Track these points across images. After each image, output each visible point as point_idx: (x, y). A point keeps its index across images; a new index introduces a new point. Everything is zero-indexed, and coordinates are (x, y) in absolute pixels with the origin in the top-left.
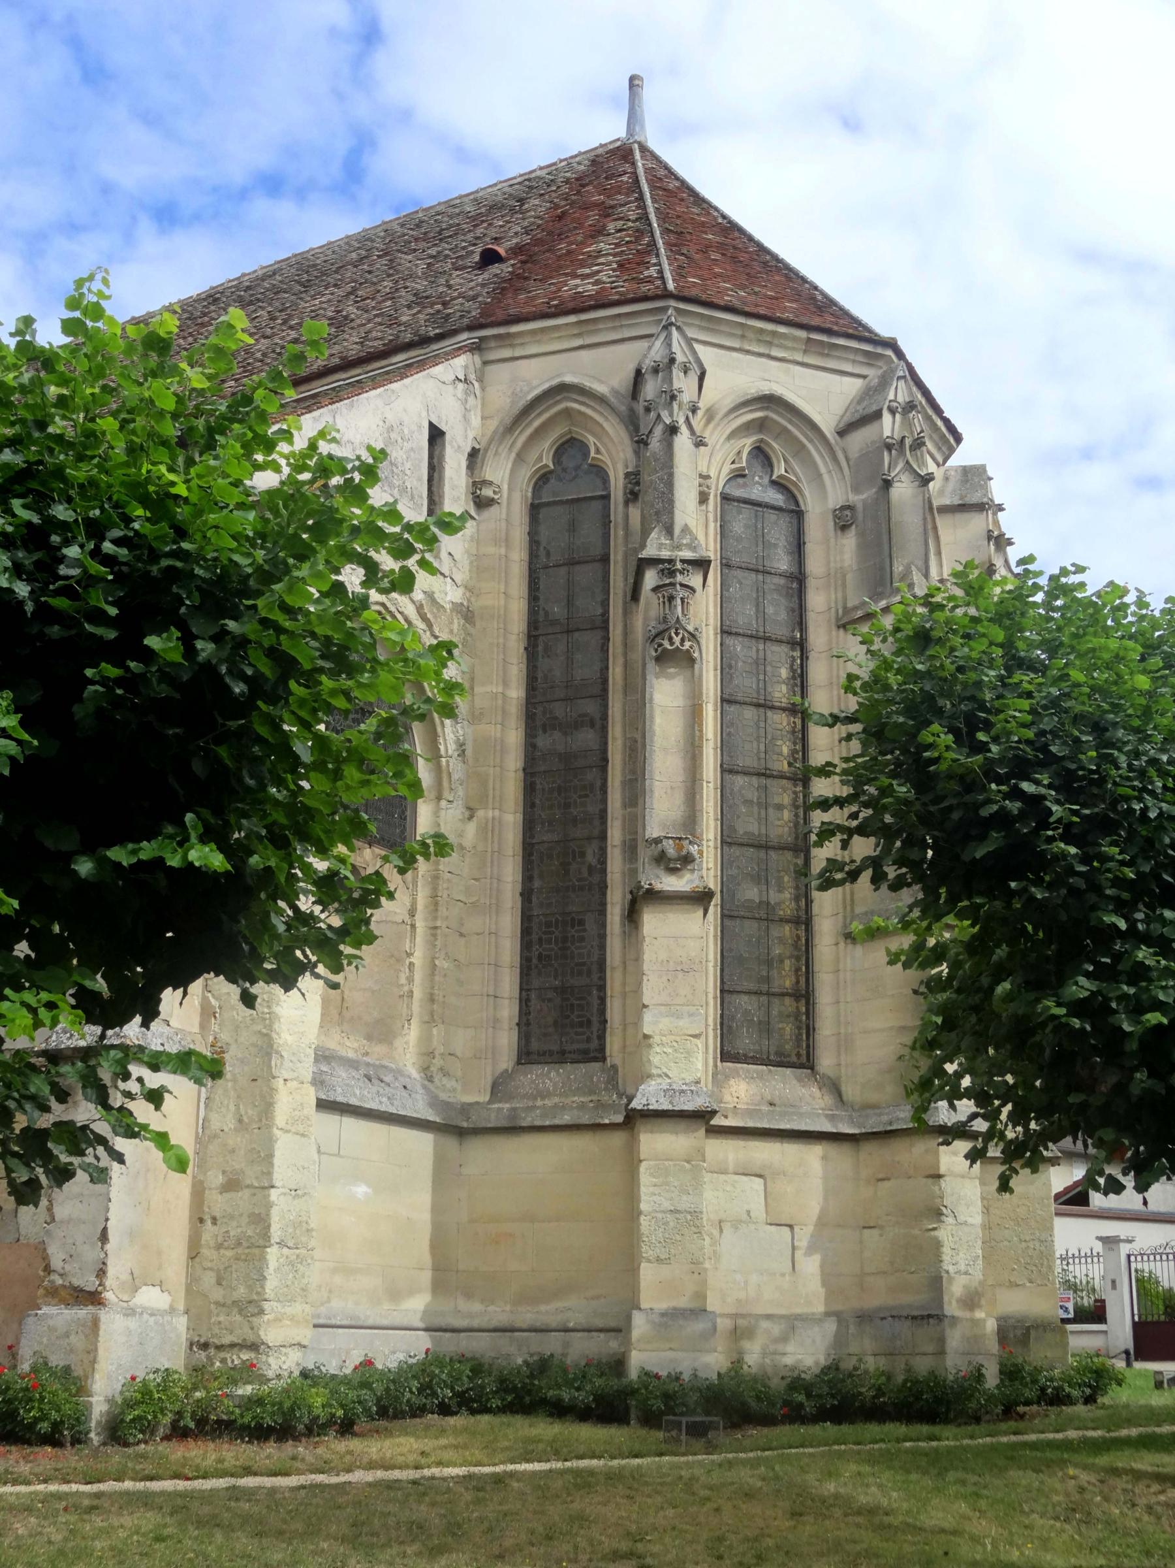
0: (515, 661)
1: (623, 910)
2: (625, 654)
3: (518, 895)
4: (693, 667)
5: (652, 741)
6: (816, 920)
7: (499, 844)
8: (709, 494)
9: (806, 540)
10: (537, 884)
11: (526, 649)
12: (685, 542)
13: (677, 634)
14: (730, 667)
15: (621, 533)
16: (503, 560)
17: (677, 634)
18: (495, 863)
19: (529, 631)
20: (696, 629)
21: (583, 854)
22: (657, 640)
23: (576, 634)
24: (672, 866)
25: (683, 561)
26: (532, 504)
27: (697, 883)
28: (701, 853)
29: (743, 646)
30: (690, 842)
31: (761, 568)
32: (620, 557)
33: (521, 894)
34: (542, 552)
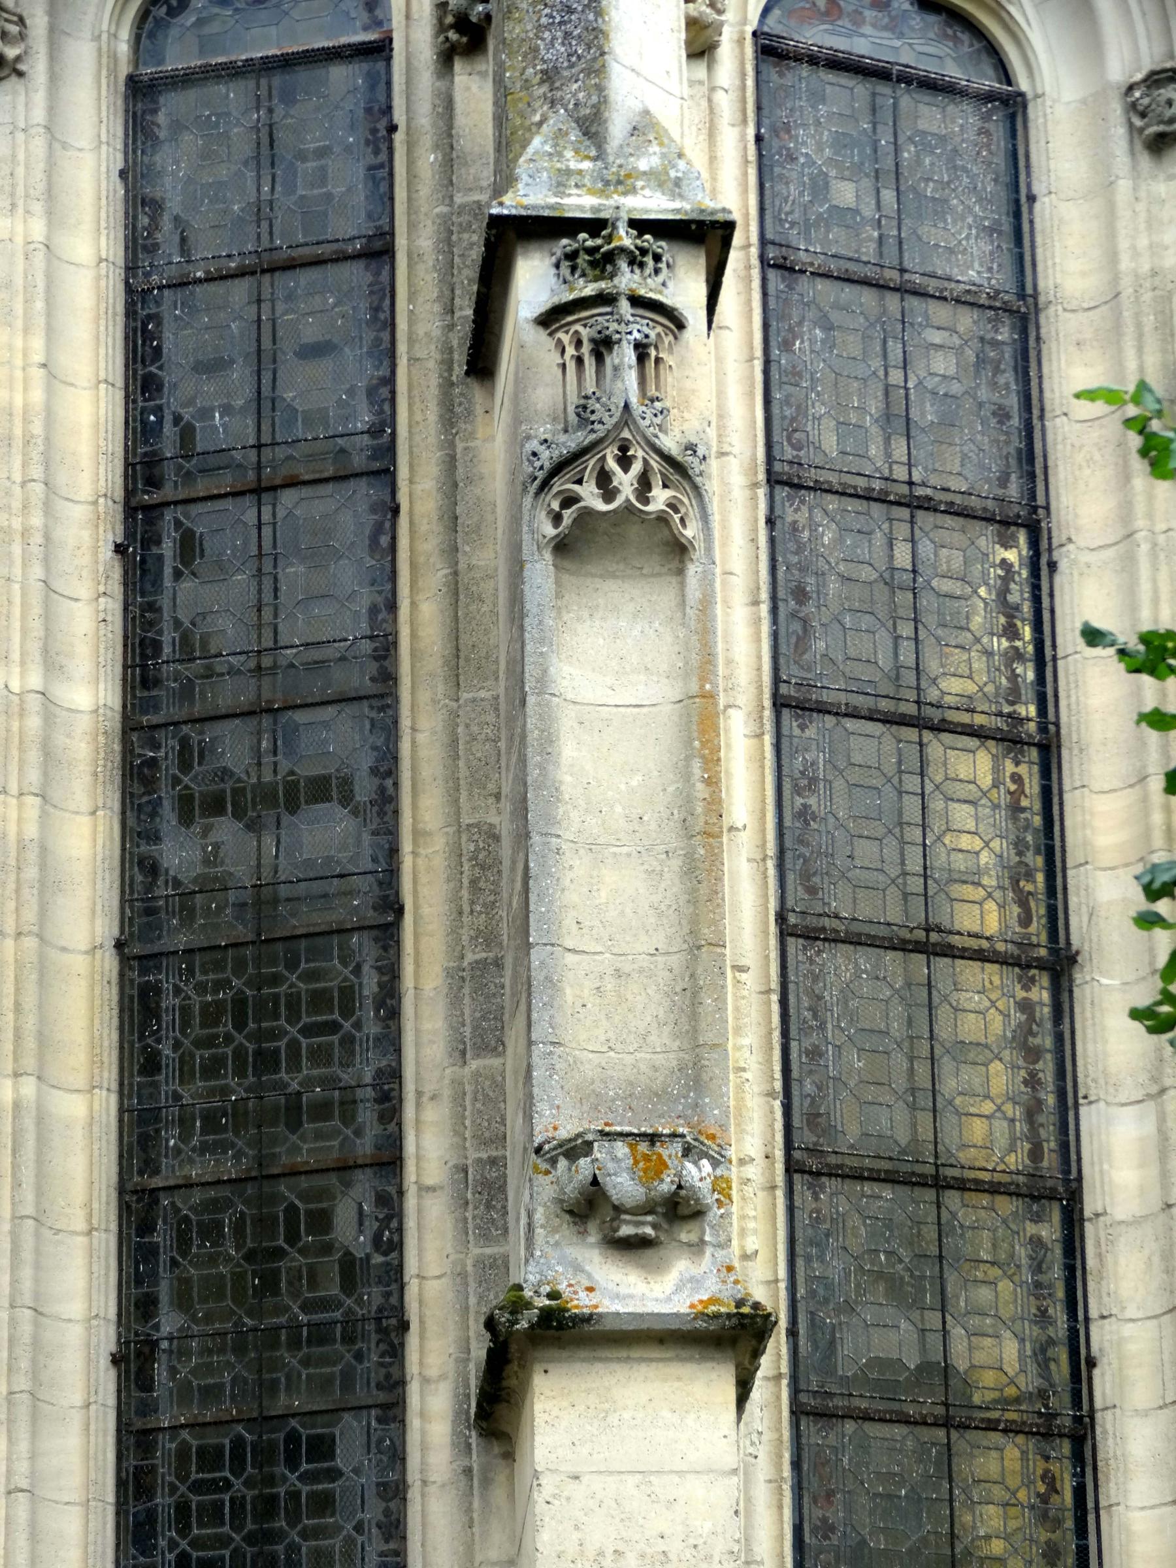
0: (84, 590)
1: (461, 1398)
2: (452, 551)
3: (104, 1361)
4: (681, 572)
5: (551, 820)
6: (1106, 1423)
7: (40, 1192)
8: (718, 28)
9: (1037, 188)
10: (169, 1322)
11: (119, 549)
12: (643, 165)
13: (625, 462)
14: (800, 594)
15: (428, 160)
16: (39, 259)
17: (625, 462)
18: (27, 1255)
19: (129, 493)
20: (691, 448)
21: (322, 1221)
22: (561, 484)
23: (288, 497)
24: (626, 1230)
25: (640, 226)
26: (131, 80)
27: (711, 1287)
28: (722, 1187)
29: (844, 530)
30: (687, 1151)
31: (892, 276)
32: (426, 242)
33: (116, 1360)
34: (166, 233)
